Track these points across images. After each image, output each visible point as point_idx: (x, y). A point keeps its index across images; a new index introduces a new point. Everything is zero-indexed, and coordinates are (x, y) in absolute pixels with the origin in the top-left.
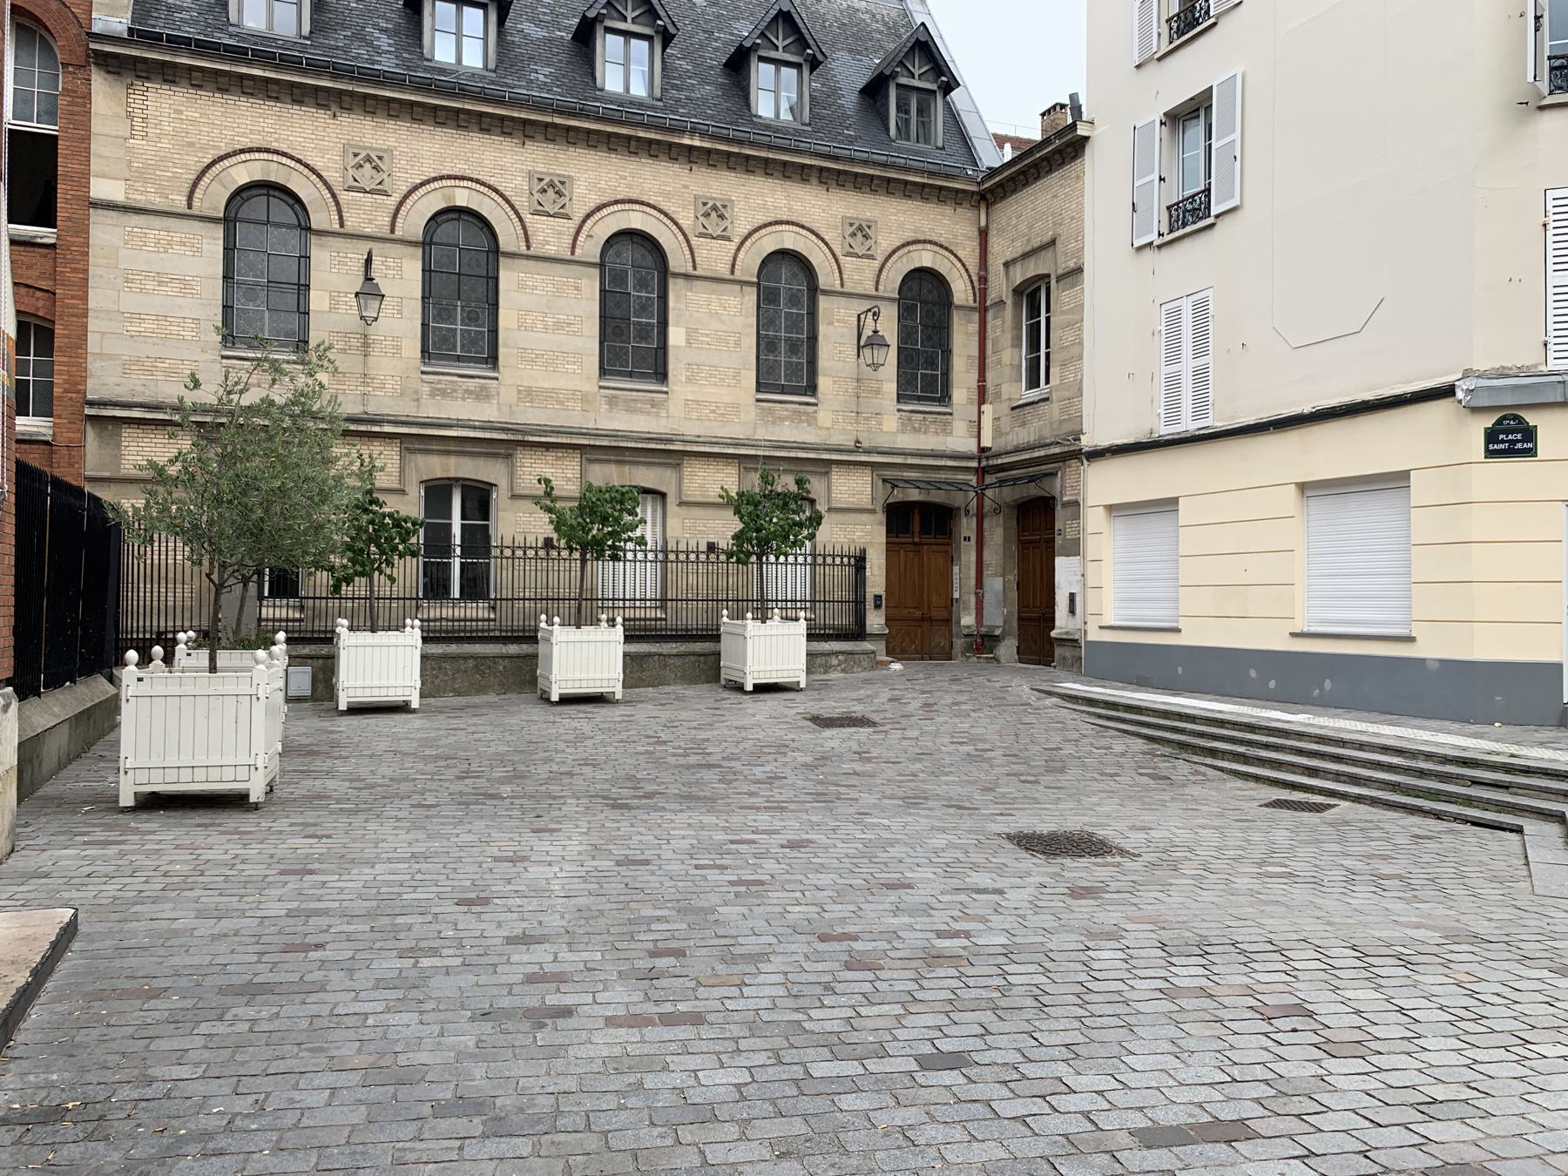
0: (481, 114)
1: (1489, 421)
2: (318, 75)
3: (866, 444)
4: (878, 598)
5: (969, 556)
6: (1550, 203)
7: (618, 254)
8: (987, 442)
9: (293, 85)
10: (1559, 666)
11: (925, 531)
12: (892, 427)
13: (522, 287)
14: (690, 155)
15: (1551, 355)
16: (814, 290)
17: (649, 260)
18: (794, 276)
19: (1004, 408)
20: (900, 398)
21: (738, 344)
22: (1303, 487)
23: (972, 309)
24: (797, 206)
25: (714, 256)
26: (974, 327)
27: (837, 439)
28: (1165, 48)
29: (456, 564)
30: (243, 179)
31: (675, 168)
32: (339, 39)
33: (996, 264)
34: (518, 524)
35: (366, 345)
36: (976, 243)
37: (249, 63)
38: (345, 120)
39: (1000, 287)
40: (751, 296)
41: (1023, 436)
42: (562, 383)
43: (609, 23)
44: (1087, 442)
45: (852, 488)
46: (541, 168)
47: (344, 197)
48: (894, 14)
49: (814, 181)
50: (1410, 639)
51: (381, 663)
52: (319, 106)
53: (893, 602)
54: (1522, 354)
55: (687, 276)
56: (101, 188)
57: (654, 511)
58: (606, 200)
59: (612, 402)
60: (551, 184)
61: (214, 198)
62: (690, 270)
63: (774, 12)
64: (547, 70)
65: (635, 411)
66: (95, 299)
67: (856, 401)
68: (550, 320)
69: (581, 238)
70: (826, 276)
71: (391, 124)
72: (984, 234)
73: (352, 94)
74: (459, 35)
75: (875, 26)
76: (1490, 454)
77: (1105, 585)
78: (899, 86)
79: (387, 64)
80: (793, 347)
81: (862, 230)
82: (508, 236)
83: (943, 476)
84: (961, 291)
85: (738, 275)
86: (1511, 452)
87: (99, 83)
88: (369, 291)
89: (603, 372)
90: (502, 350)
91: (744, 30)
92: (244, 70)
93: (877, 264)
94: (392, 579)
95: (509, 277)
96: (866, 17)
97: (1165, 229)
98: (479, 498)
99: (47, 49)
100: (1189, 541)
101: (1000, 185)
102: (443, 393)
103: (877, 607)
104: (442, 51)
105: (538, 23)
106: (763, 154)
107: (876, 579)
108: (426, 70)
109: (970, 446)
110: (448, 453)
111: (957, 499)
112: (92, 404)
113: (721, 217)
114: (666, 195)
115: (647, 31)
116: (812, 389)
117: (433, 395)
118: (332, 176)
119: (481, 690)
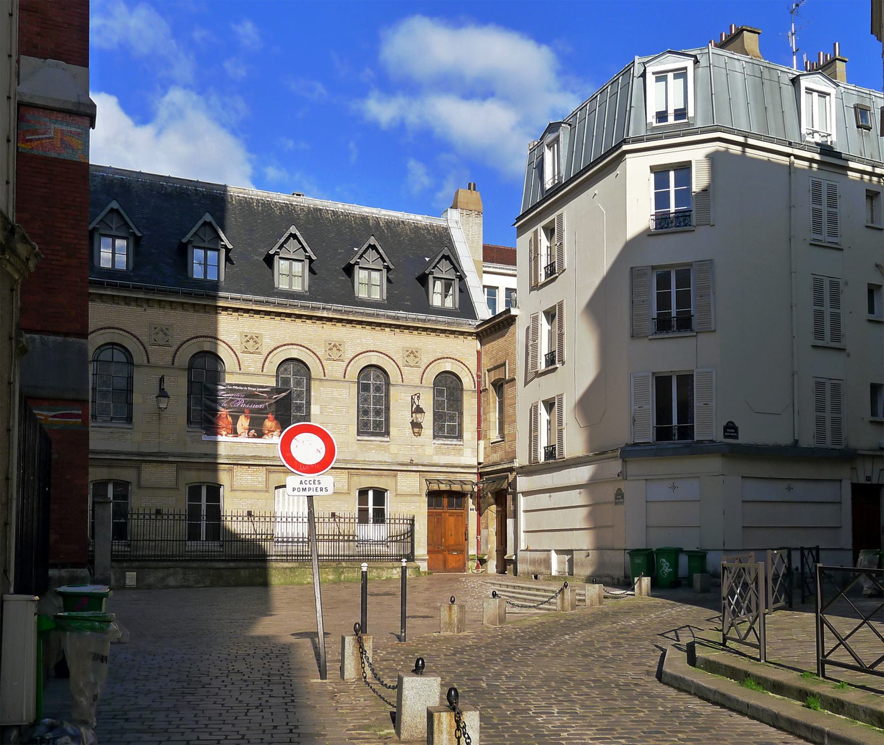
7: (286, 370)
8: (481, 460)
29: (203, 524)
33: (484, 370)
37: (105, 289)
38: (150, 311)
40: (355, 387)
47: (149, 348)
52: (138, 306)
55: (321, 380)
62: (323, 377)
80: (378, 413)
84: (468, 383)
93: (421, 370)
116: (387, 433)
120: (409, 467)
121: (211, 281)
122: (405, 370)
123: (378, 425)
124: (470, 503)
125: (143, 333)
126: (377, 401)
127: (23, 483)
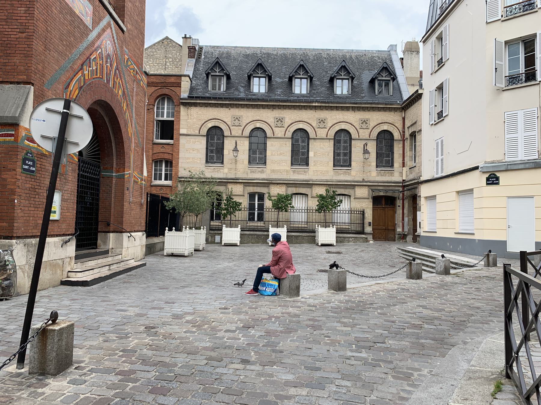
0: (263, 105)
1: (487, 175)
2: (226, 101)
3: (366, 180)
4: (370, 223)
5: (399, 211)
6: (506, 116)
7: (297, 135)
8: (404, 179)
9: (221, 104)
10: (505, 242)
11: (386, 204)
12: (375, 175)
13: (272, 145)
14: (315, 108)
15: (506, 157)
16: (351, 139)
17: (305, 136)
18: (346, 135)
19: (408, 168)
20: (377, 167)
21: (328, 155)
22: (458, 192)
23: (400, 140)
24: (346, 117)
25: (322, 133)
26: (401, 145)
27: (357, 179)
28: (437, 68)
29: (256, 213)
30: (210, 126)
31: (312, 111)
32: (232, 91)
33: (406, 127)
34: (268, 204)
35: (236, 162)
36: (401, 122)
37: (211, 100)
38: (232, 110)
39: (407, 135)
40: (332, 142)
41: (411, 177)
42: (282, 168)
43: (296, 76)
44: (422, 179)
45: (362, 192)
46: (277, 116)
47: (231, 128)
48: (386, 56)
49: (351, 110)
50: (473, 234)
51: (231, 234)
52: (227, 107)
53: (375, 223)
54: (498, 157)
55: (314, 139)
56: (182, 131)
57: (303, 199)
58: (293, 122)
59: (294, 172)
60: (280, 120)
61: (204, 131)
62: (315, 137)
63: (340, 66)
64: (280, 91)
65: (300, 174)
66: (181, 155)
67: (364, 167)
68: (279, 153)
69: (287, 132)
70: (354, 135)
71: (242, 109)
72: (404, 119)
73: (233, 104)
74: (259, 85)
75: (379, 61)
76: (487, 184)
77: (428, 220)
78: (378, 80)
79: (242, 95)
80: (345, 155)
81: (365, 122)
82: (269, 133)
83: (391, 188)
84: (397, 135)
85: (328, 137)
86: (493, 184)
87: (182, 108)
88: (236, 150)
89: (292, 164)
90: (267, 161)
91: (330, 73)
92: (210, 102)
93: (370, 130)
94: (235, 216)
95: (269, 143)
96: (377, 59)
97: (436, 119)
98: (261, 197)
99: (173, 101)
100: (439, 207)
101: (406, 105)
102: (253, 172)
103: (370, 225)
104: (255, 90)
105: (280, 77)
106: (335, 105)
107: (369, 216)
108: (251, 95)
109: (400, 180)
110: (254, 186)
111: (396, 195)
112: (179, 178)
113: (324, 122)
114: (309, 119)
115: (306, 77)
116: (350, 165)
117: (251, 173)
118: (229, 123)
119: (258, 243)
120: (362, 184)
121: (345, 95)
122: (361, 131)
123: (339, 161)
124: (399, 203)
125: (228, 120)
126: (345, 148)
127: (109, 193)
